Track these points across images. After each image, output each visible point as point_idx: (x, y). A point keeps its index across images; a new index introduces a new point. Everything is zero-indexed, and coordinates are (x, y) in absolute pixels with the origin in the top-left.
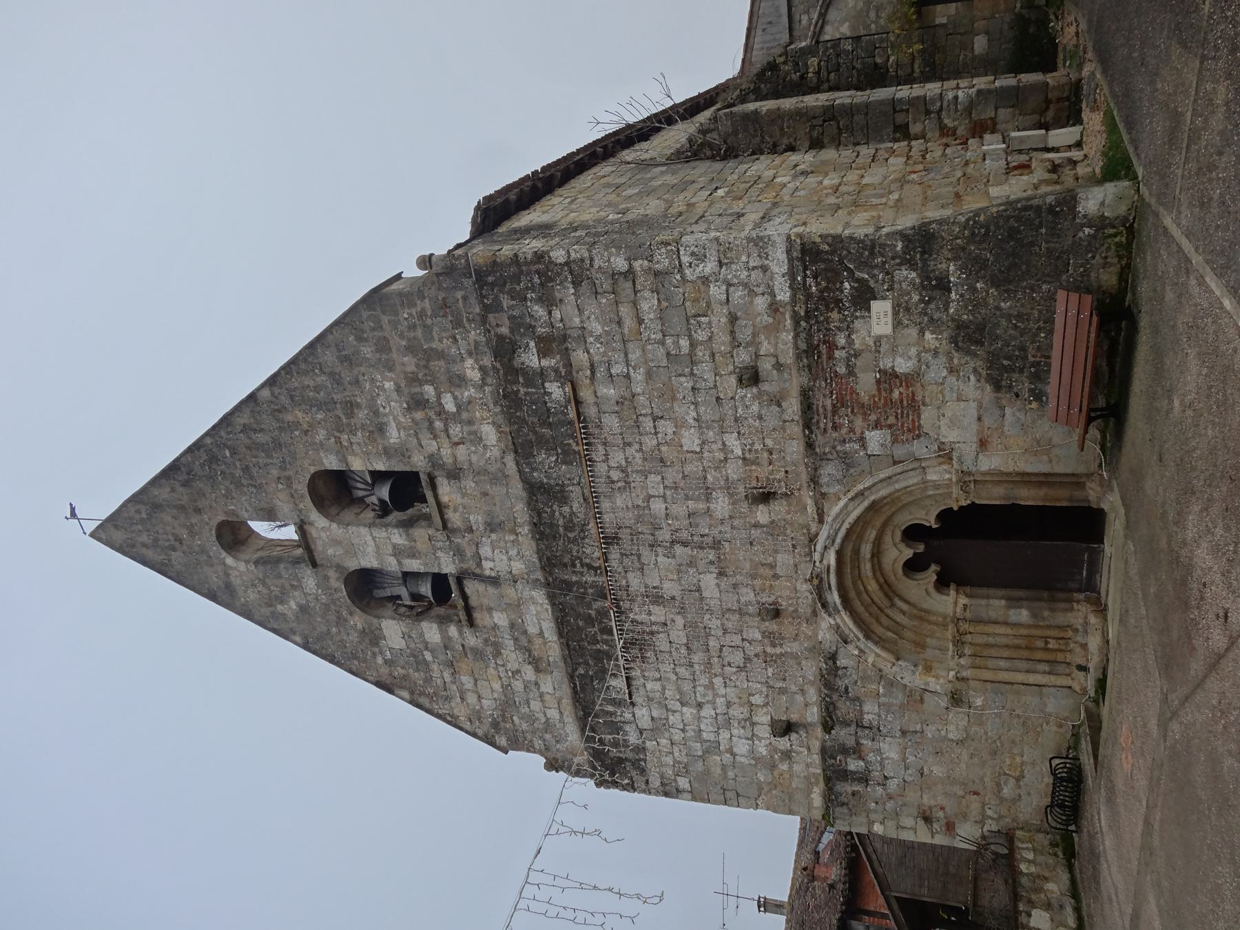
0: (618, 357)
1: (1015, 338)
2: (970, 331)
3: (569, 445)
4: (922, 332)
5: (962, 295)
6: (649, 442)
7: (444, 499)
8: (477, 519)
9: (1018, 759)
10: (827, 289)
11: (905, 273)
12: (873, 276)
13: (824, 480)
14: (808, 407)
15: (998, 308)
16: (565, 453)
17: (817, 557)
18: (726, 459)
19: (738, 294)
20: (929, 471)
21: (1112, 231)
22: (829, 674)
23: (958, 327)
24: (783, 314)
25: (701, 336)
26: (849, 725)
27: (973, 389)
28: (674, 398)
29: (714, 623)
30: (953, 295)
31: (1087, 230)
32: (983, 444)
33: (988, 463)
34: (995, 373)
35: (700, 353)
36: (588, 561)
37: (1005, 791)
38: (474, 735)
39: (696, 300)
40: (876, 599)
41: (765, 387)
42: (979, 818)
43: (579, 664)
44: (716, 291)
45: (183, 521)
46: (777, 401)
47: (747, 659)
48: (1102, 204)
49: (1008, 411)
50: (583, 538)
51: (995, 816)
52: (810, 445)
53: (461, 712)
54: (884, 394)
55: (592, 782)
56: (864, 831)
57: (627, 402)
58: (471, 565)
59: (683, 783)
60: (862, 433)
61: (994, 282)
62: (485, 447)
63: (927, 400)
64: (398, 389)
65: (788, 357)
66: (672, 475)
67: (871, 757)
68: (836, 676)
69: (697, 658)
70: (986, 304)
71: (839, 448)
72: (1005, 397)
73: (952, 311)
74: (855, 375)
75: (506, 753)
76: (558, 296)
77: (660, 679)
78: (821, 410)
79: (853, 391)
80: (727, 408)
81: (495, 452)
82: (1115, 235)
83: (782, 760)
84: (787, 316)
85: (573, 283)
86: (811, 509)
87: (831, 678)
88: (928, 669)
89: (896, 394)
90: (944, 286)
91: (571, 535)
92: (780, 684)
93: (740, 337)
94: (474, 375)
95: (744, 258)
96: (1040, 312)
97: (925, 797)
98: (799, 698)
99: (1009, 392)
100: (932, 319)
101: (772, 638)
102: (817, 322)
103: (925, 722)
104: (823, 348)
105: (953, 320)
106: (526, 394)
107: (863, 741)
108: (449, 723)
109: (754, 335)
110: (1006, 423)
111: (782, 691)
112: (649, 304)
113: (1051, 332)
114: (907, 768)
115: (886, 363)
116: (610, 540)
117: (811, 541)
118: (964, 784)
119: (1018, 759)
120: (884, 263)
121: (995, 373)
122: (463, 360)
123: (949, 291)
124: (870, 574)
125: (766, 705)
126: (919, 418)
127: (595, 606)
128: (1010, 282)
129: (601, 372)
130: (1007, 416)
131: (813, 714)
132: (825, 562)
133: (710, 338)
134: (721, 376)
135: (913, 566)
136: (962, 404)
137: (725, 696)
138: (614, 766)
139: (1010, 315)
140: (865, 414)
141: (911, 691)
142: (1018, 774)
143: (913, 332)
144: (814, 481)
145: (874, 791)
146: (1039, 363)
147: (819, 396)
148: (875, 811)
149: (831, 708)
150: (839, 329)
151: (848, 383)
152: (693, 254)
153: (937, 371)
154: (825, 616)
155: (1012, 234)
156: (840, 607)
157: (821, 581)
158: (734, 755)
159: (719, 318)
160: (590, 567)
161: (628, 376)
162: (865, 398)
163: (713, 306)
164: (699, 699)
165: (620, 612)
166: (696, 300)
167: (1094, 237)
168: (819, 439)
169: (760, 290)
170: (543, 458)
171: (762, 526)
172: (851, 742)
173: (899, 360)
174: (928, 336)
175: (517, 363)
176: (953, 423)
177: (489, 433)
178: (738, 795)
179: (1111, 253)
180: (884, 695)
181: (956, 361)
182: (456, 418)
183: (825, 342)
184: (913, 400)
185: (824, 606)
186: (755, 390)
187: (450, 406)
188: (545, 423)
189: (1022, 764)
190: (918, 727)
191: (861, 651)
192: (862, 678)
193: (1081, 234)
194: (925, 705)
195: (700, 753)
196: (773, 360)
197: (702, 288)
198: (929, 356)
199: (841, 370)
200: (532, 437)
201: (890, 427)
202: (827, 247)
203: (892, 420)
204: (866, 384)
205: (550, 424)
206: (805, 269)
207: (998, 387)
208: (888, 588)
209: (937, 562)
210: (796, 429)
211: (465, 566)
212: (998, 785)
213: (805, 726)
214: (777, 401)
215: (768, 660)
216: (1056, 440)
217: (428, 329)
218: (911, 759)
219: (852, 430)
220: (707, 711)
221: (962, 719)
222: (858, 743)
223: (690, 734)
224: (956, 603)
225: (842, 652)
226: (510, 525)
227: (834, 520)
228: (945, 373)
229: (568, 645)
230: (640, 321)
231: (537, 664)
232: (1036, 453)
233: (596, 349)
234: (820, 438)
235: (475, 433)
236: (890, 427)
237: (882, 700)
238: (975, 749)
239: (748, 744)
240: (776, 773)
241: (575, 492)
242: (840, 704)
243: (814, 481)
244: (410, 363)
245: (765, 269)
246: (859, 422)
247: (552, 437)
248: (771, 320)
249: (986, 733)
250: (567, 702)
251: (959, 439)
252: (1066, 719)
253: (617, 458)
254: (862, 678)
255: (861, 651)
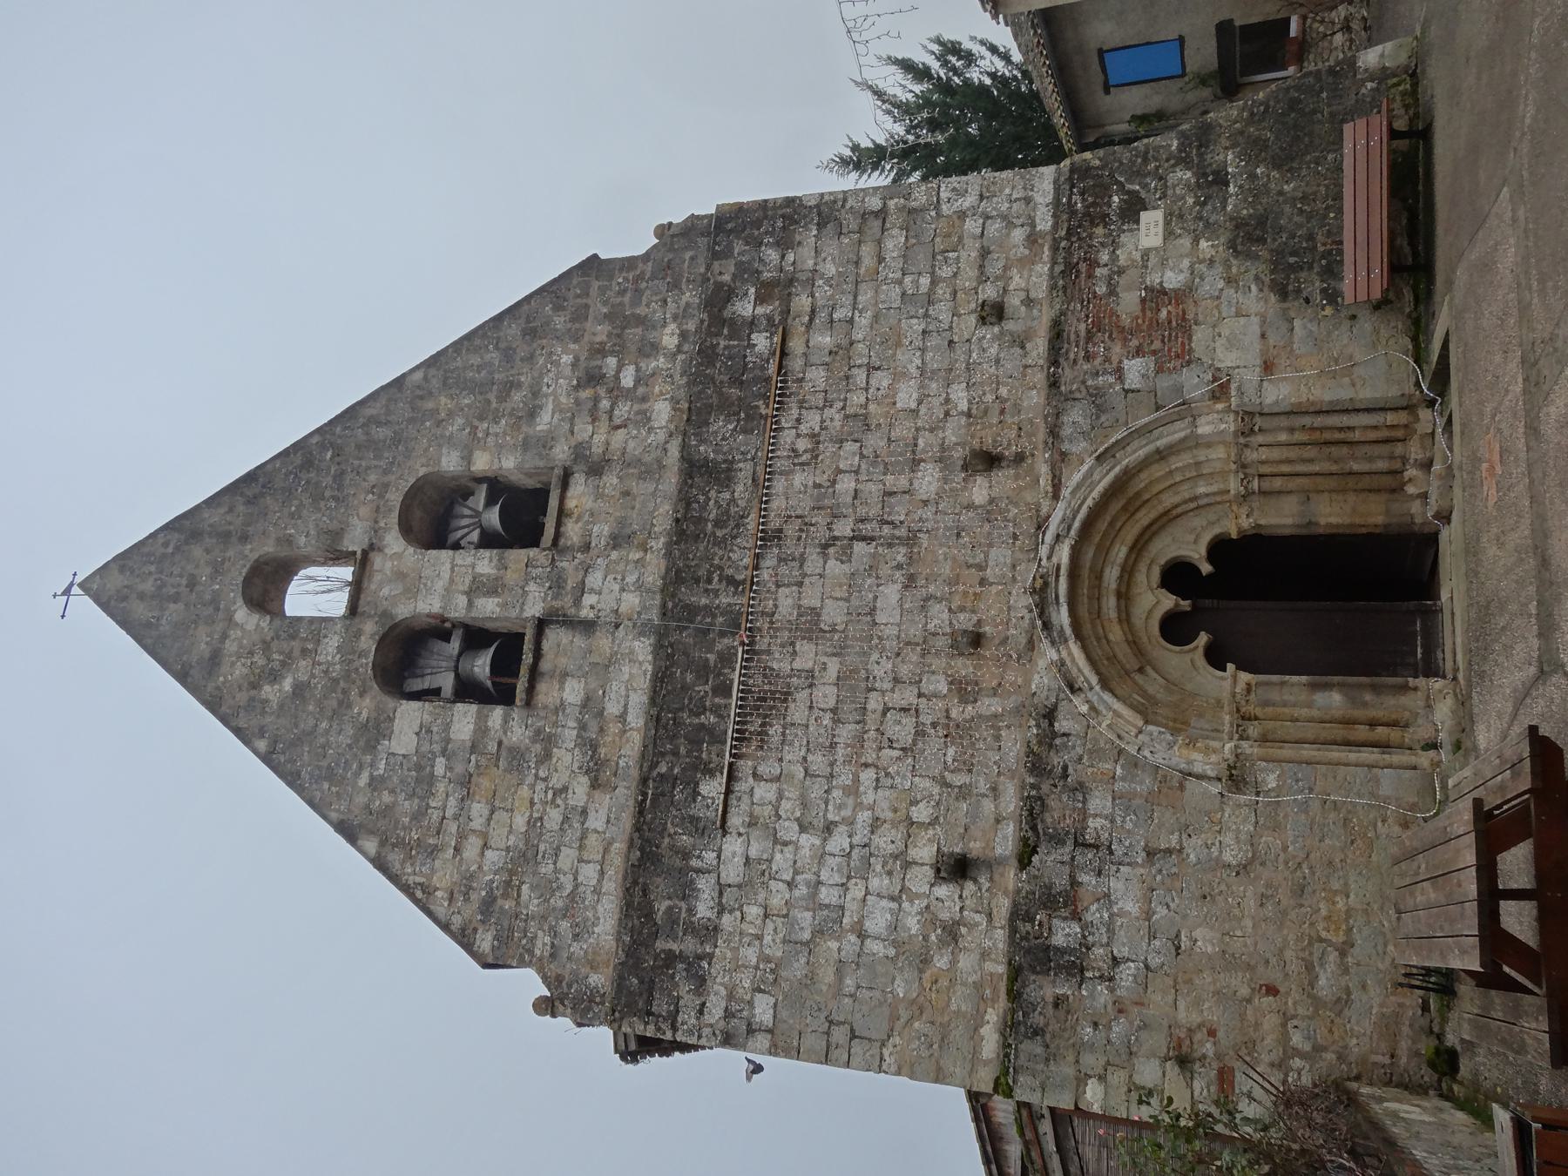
0: (847, 300)
1: (1300, 226)
2: (1250, 229)
3: (757, 407)
4: (1196, 241)
5: (1241, 187)
6: (857, 399)
7: (571, 504)
8: (602, 530)
9: (1341, 904)
10: (1094, 204)
11: (1179, 174)
12: (1145, 186)
13: (1067, 431)
14: (1057, 334)
15: (1281, 193)
16: (749, 418)
17: (1044, 551)
18: (947, 414)
19: (994, 228)
20: (1201, 420)
21: (1395, 80)
22: (1040, 743)
23: (1237, 227)
24: (1042, 246)
25: (946, 272)
26: (1061, 842)
27: (1255, 301)
28: (898, 344)
29: (881, 669)
30: (1232, 189)
31: (1369, 85)
32: (1268, 367)
33: (1277, 393)
34: (1280, 277)
35: (942, 291)
36: (730, 572)
37: (1322, 982)
38: (445, 927)
39: (948, 235)
40: (1120, 656)
41: (1009, 325)
42: (1275, 1056)
43: (663, 754)
44: (972, 226)
45: (194, 590)
46: (1021, 342)
47: (920, 733)
48: (1382, 56)
49: (1297, 323)
50: (735, 537)
51: (1307, 1047)
52: (1054, 384)
53: (444, 875)
54: (1149, 313)
55: (603, 1036)
56: (1065, 1102)
57: (841, 352)
58: (566, 602)
59: (763, 1010)
60: (1120, 362)
61: (1277, 163)
62: (651, 429)
63: (1201, 318)
64: (574, 365)
65: (1040, 291)
66: (875, 441)
67: (1094, 914)
68: (1051, 746)
69: (845, 733)
70: (1268, 192)
71: (1089, 383)
72: (1294, 305)
73: (1229, 208)
74: (1117, 295)
75: (661, 231)
76: (798, 238)
77: (778, 779)
78: (1073, 337)
79: (1113, 313)
80: (960, 353)
81: (661, 436)
82: (1398, 84)
83: (942, 943)
84: (1046, 249)
85: (818, 224)
86: (1045, 482)
87: (1042, 751)
88: (1191, 743)
89: (1164, 314)
90: (1221, 179)
91: (719, 533)
92: (959, 779)
93: (989, 270)
94: (669, 339)
95: (1007, 191)
96: (1327, 187)
97: (1182, 1004)
98: (988, 806)
99: (1296, 299)
100: (1208, 225)
101: (965, 690)
102: (1080, 239)
103: (1185, 829)
104: (1083, 267)
105: (1231, 219)
106: (726, 347)
107: (1083, 878)
108: (416, 901)
109: (1006, 268)
110: (1296, 339)
111: (964, 792)
112: (895, 242)
113: (1340, 211)
114: (1152, 936)
115: (1154, 279)
116: (770, 537)
117: (1039, 528)
118: (1250, 967)
119: (1341, 904)
120: (1157, 168)
121: (1280, 277)
122: (665, 325)
123: (1227, 184)
124: (1113, 614)
125: (934, 822)
126: (1190, 339)
127: (719, 647)
128: (1292, 160)
129: (822, 315)
130: (1297, 329)
131: (1006, 842)
132: (1055, 560)
133: (955, 275)
134: (959, 316)
135: (1175, 629)
136: (1242, 320)
137: (872, 808)
138: (646, 997)
139: (1294, 199)
140: (1125, 339)
141: (1165, 777)
142: (1341, 938)
143: (1185, 242)
144: (1054, 432)
145: (1092, 995)
146: (1330, 252)
147: (1072, 319)
148: (1092, 1047)
149: (1037, 809)
150: (1102, 244)
151: (1107, 304)
152: (954, 189)
153: (1212, 282)
154: (1045, 644)
155: (1293, 105)
156: (1068, 631)
157: (1046, 584)
158: (862, 936)
159: (970, 253)
160: (731, 581)
161: (851, 321)
162: (1126, 321)
163: (966, 241)
164: (831, 817)
165: (751, 652)
166: (948, 235)
167: (1377, 89)
168: (1067, 373)
169: (1018, 222)
170: (721, 426)
171: (976, 508)
172: (1061, 882)
173: (1169, 274)
174: (1204, 244)
175: (726, 314)
176: (1232, 343)
177: (662, 412)
178: (853, 1036)
179: (1397, 105)
180: (1123, 779)
181: (1234, 270)
182: (628, 394)
183: (1085, 260)
184: (1184, 319)
185: (1047, 626)
186: (996, 329)
187: (627, 380)
188: (737, 382)
189: (1349, 912)
190: (1174, 841)
191: (1093, 708)
192: (1090, 752)
193: (1363, 91)
194: (1187, 793)
195: (806, 936)
196: (1023, 295)
197: (957, 222)
198: (1203, 267)
199: (1101, 289)
200: (715, 400)
201: (1154, 353)
202: (1097, 162)
203: (1157, 345)
204: (1128, 303)
205: (742, 383)
206: (1073, 186)
207: (1283, 293)
208: (1134, 644)
209: (1210, 575)
210: (1039, 378)
211: (557, 604)
212: (1309, 967)
213: (990, 864)
214: (1021, 342)
215: (953, 731)
216: (1358, 357)
217: (638, 292)
218: (1161, 912)
219: (1107, 360)
220: (839, 841)
221: (1245, 820)
222: (1074, 883)
223: (802, 891)
224: (1235, 678)
225: (1063, 707)
226: (640, 537)
227: (1073, 493)
228: (1221, 284)
229: (658, 719)
230: (881, 260)
231: (597, 774)
232: (1334, 375)
233: (823, 292)
234: (1068, 371)
235: (644, 412)
236: (1154, 353)
237: (1119, 786)
238: (1268, 886)
239: (891, 908)
240: (927, 975)
241: (745, 471)
242: (1052, 803)
243: (1054, 432)
244: (600, 332)
245: (1028, 200)
246: (1117, 349)
247: (740, 399)
248: (1027, 252)
249: (1285, 849)
250: (617, 861)
251: (1238, 363)
252: (1413, 807)
253: (812, 421)
254: (1090, 752)
255: (1093, 708)
